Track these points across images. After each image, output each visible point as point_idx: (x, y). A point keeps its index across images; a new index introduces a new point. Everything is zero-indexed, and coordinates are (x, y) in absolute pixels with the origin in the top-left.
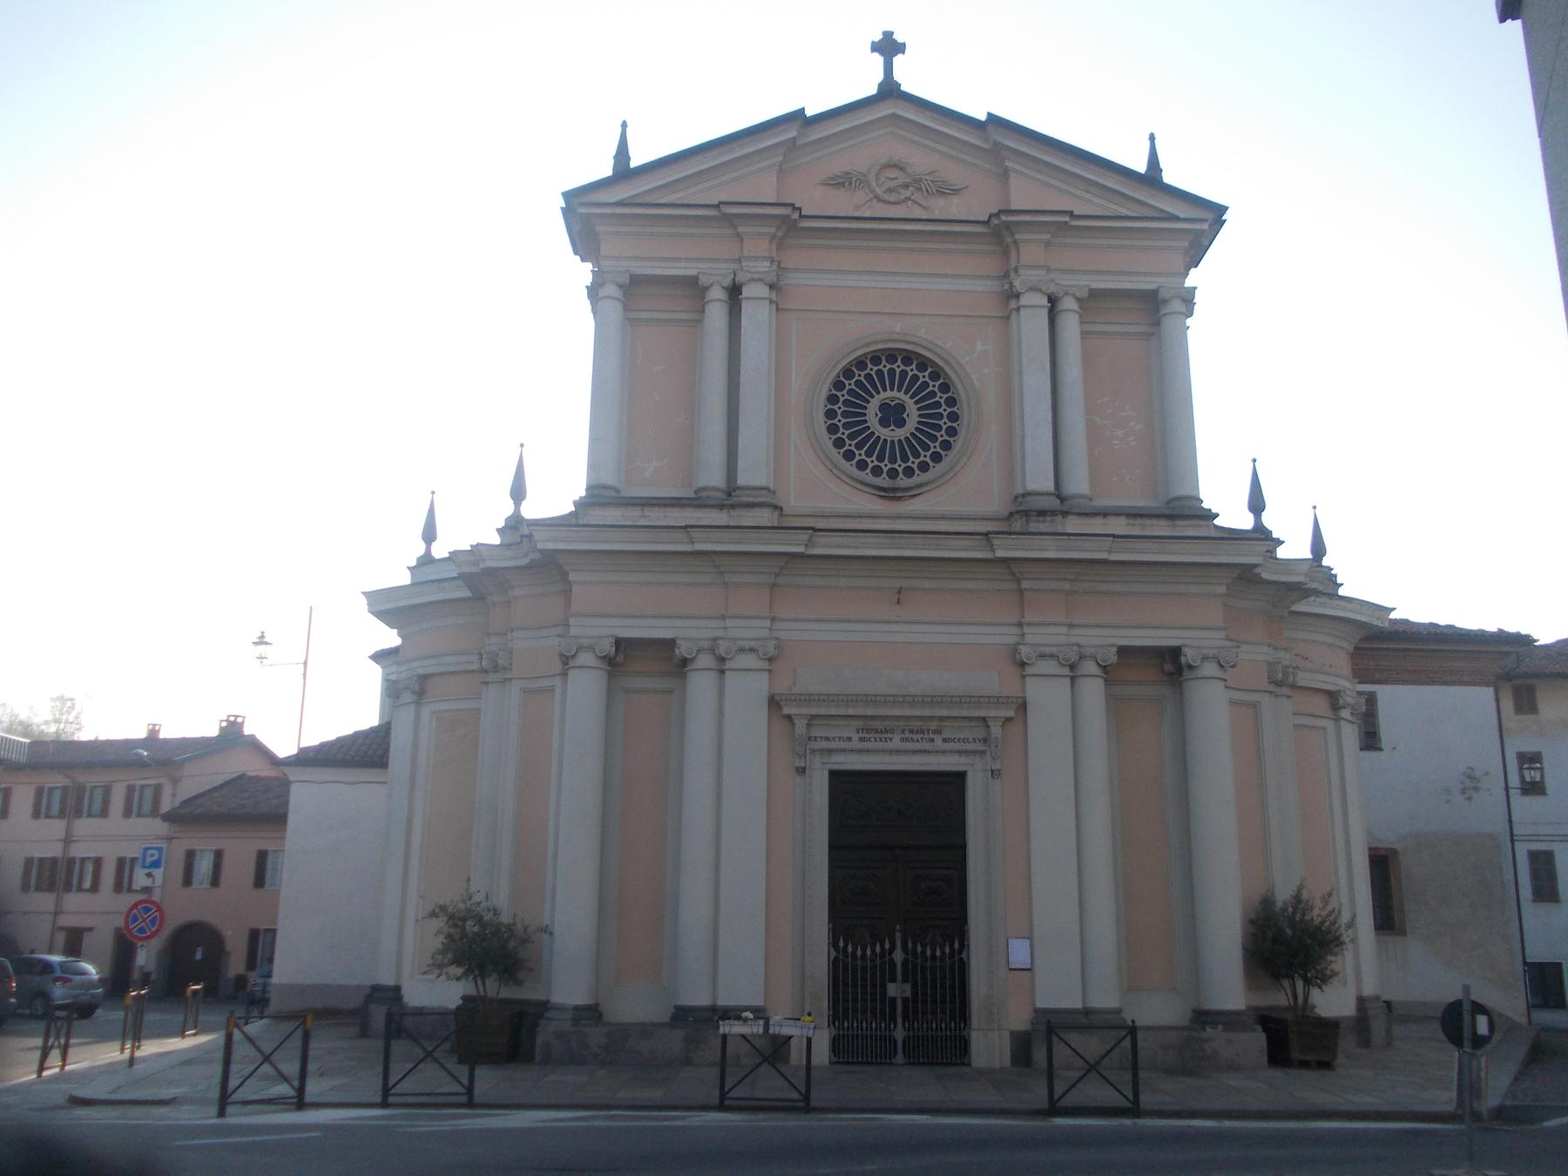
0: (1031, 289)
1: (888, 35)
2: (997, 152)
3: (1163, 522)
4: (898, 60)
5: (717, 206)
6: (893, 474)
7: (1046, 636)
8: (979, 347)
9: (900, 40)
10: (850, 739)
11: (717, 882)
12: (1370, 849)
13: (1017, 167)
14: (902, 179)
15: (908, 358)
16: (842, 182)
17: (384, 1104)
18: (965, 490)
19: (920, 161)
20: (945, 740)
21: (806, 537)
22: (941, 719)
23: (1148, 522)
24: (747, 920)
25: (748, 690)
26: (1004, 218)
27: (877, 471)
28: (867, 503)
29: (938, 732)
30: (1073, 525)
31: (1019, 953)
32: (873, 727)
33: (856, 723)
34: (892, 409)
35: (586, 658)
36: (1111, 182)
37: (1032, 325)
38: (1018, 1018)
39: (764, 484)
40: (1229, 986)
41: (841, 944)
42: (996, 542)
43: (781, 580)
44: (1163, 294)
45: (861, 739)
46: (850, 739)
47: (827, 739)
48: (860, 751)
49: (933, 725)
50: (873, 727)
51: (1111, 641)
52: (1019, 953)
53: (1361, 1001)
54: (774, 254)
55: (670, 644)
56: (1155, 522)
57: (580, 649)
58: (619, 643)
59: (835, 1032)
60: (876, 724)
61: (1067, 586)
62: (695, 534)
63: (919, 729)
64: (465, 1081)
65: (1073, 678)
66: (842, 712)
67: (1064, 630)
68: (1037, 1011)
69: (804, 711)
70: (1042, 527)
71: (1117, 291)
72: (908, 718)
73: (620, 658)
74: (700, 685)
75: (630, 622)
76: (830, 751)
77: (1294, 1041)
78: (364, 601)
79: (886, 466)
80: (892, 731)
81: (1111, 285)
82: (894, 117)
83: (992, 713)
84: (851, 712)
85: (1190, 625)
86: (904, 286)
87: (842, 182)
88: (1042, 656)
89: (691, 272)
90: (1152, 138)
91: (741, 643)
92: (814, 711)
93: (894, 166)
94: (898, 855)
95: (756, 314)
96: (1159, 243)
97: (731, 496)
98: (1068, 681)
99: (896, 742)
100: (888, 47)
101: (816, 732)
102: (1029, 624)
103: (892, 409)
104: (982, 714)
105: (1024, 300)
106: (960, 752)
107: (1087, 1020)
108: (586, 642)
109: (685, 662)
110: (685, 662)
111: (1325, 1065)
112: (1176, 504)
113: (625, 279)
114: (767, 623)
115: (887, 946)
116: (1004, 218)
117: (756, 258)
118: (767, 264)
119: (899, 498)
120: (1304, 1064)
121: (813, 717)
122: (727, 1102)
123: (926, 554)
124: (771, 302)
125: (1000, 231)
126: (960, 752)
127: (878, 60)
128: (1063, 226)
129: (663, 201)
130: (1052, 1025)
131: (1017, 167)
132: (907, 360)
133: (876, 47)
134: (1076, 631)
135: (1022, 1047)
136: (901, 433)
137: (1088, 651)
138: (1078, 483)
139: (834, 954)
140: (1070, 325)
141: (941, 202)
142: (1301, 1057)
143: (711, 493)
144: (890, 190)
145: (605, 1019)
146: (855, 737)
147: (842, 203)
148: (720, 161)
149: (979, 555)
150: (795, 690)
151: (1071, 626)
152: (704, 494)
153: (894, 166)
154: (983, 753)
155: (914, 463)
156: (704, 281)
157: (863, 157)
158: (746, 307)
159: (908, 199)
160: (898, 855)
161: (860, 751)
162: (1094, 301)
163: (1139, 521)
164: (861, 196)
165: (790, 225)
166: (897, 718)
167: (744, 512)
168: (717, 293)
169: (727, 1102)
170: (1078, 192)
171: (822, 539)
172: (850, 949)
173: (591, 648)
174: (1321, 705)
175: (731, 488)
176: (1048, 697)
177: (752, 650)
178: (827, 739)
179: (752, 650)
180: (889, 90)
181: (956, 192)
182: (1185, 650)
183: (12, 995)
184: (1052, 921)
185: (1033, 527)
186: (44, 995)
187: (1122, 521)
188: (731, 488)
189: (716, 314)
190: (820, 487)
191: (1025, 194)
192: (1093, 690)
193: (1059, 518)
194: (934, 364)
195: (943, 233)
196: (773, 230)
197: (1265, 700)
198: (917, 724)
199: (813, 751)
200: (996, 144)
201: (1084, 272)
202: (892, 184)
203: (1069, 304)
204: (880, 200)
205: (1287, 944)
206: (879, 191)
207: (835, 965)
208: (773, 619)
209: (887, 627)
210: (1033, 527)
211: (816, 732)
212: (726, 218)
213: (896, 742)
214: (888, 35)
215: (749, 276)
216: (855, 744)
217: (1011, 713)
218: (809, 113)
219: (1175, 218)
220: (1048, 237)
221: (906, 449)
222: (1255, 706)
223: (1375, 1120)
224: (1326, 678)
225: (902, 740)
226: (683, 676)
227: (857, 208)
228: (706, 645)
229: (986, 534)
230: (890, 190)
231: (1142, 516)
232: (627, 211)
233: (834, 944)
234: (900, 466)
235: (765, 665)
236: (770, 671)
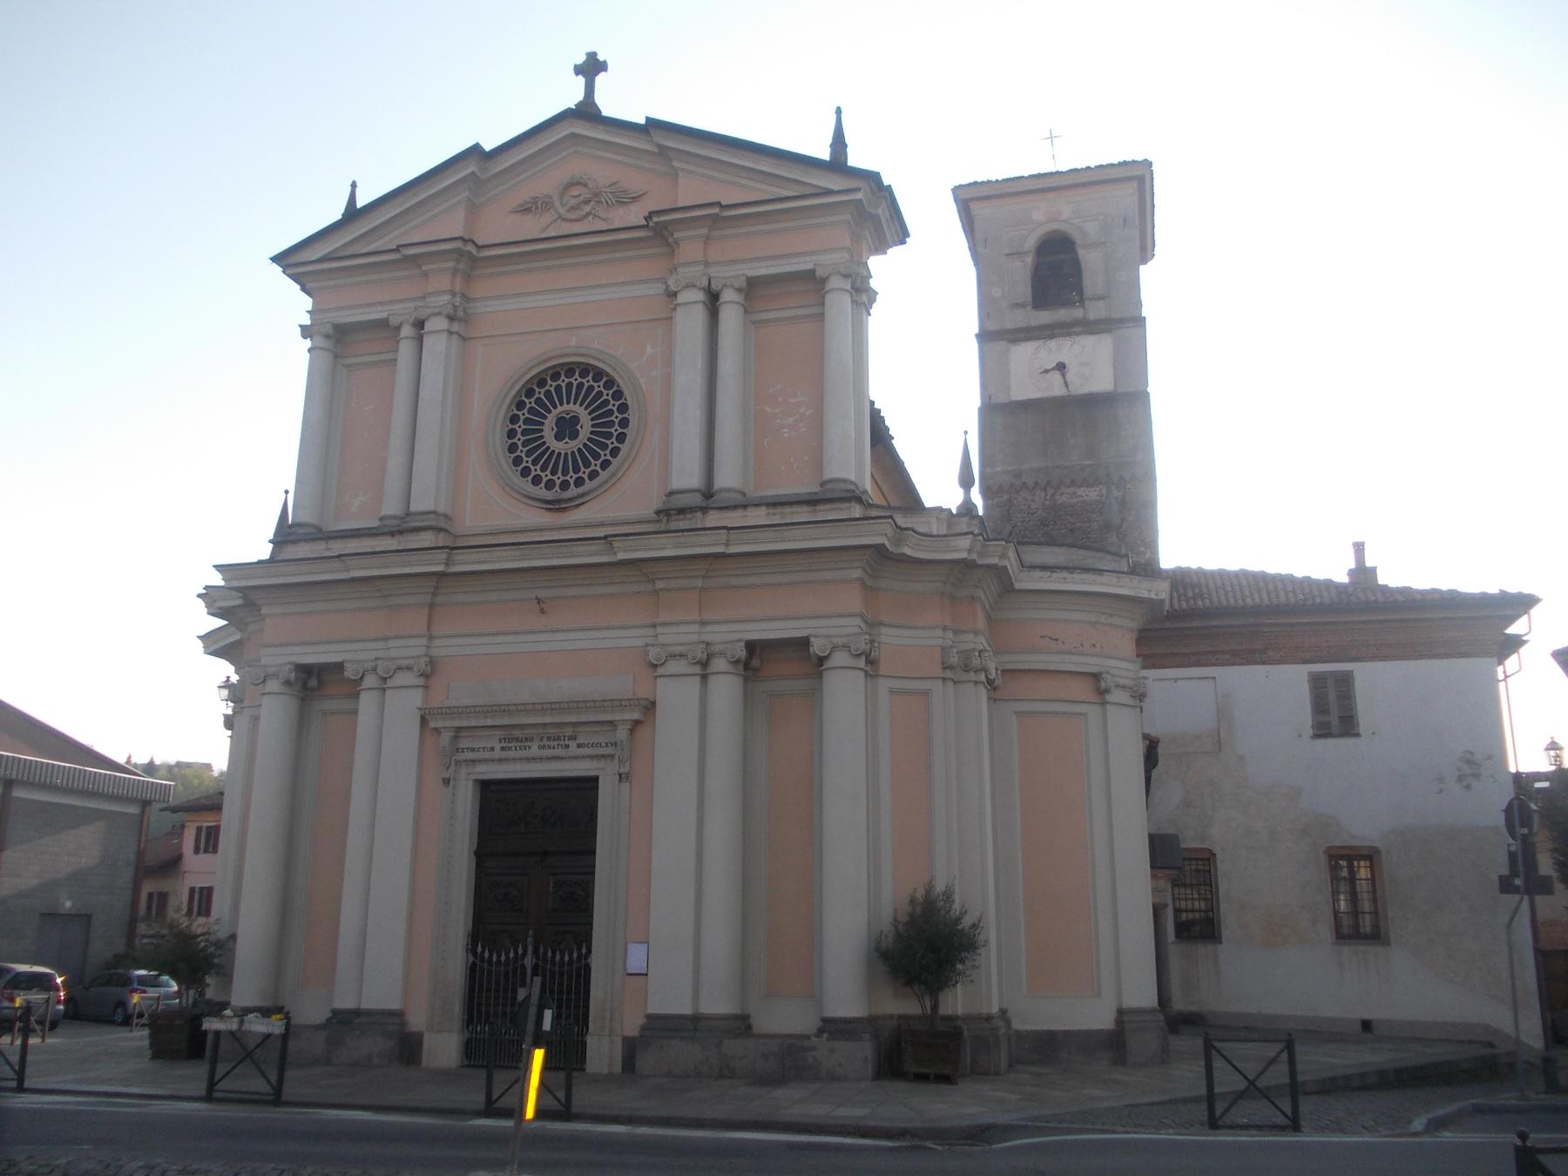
0: (687, 287)
1: (592, 56)
2: (663, 153)
3: (805, 509)
4: (600, 79)
5: (397, 249)
6: (565, 486)
7: (682, 635)
8: (649, 350)
9: (584, 58)
10: (492, 749)
11: (367, 892)
12: (1153, 839)
13: (686, 166)
14: (585, 194)
15: (585, 370)
16: (525, 209)
17: (209, 1098)
18: (624, 497)
19: (602, 173)
20: (579, 746)
21: (444, 556)
22: (575, 724)
23: (787, 509)
24: (390, 923)
25: (405, 704)
26: (655, 219)
27: (550, 485)
28: (536, 517)
29: (573, 738)
30: (713, 519)
31: (636, 958)
32: (513, 736)
33: (499, 733)
34: (567, 420)
35: (719, 664)
36: (765, 166)
37: (690, 321)
38: (631, 1025)
39: (431, 508)
40: (846, 989)
41: (479, 949)
42: (616, 545)
43: (439, 599)
44: (820, 273)
45: (503, 749)
46: (492, 749)
47: (473, 750)
48: (500, 760)
49: (569, 731)
50: (513, 736)
51: (738, 636)
52: (636, 958)
53: (1121, 1012)
54: (458, 288)
55: (804, 642)
56: (795, 509)
57: (834, 648)
58: (751, 646)
59: (467, 1036)
60: (517, 733)
61: (699, 583)
62: (734, 535)
63: (557, 735)
64: (274, 1078)
65: (704, 677)
66: (481, 723)
67: (696, 628)
68: (650, 1017)
69: (449, 723)
70: (683, 525)
71: (772, 276)
72: (545, 725)
73: (755, 662)
74: (367, 702)
75: (308, 649)
76: (473, 761)
77: (922, 1050)
78: (200, 644)
79: (571, 477)
80: (532, 740)
81: (772, 271)
82: (573, 135)
83: (617, 717)
84: (489, 722)
85: (824, 614)
86: (581, 299)
87: (525, 209)
88: (672, 656)
89: (384, 315)
90: (839, 111)
91: (399, 662)
92: (457, 724)
93: (578, 183)
94: (535, 857)
95: (437, 346)
96: (815, 221)
97: (401, 526)
98: (697, 679)
99: (534, 750)
100: (591, 68)
101: (464, 744)
102: (664, 624)
103: (567, 420)
104: (609, 717)
105: (681, 298)
106: (591, 757)
107: (690, 1026)
108: (840, 641)
109: (821, 660)
110: (821, 660)
111: (946, 1079)
112: (829, 486)
113: (328, 329)
114: (424, 641)
115: (520, 951)
116: (655, 219)
117: (438, 293)
118: (447, 297)
119: (564, 510)
120: (921, 1078)
121: (459, 729)
122: (216, 1095)
123: (555, 562)
124: (450, 333)
125: (660, 232)
126: (591, 757)
127: (581, 81)
128: (718, 218)
129: (365, 251)
130: (661, 1027)
131: (686, 166)
132: (570, 372)
133: (579, 70)
134: (709, 628)
135: (631, 1049)
136: (574, 445)
137: (717, 648)
138: (728, 477)
139: (471, 959)
140: (731, 317)
141: (621, 211)
142: (915, 1069)
143: (727, 495)
144: (573, 208)
145: (756, 1030)
146: (498, 746)
147: (531, 227)
148: (407, 205)
149: (605, 559)
150: (448, 703)
151: (702, 623)
152: (829, 486)
153: (578, 183)
154: (612, 756)
155: (584, 473)
156: (393, 322)
157: (546, 182)
158: (427, 341)
159: (589, 214)
160: (535, 857)
161: (500, 760)
162: (753, 289)
163: (779, 510)
164: (547, 218)
165: (470, 258)
166: (534, 726)
167: (411, 537)
168: (407, 331)
169: (216, 1095)
170: (743, 181)
171: (459, 556)
172: (487, 955)
173: (275, 675)
174: (1081, 689)
175: (708, 493)
176: (677, 697)
177: (682, 655)
178: (473, 750)
179: (682, 655)
180: (586, 111)
181: (635, 199)
182: (812, 639)
183: (59, 1002)
184: (670, 927)
185: (674, 525)
186: (122, 1004)
187: (763, 511)
188: (708, 493)
189: (406, 350)
190: (494, 504)
191: (692, 190)
192: (726, 688)
193: (699, 514)
194: (608, 375)
195: (612, 244)
196: (451, 264)
197: (936, 687)
198: (552, 731)
199: (458, 763)
200: (660, 146)
201: (744, 261)
202: (573, 202)
203: (728, 295)
204: (564, 220)
205: (926, 947)
206: (562, 211)
207: (472, 970)
208: (431, 638)
209: (532, 637)
210: (674, 525)
211: (464, 744)
212: (409, 260)
213: (534, 750)
214: (592, 56)
215: (429, 311)
216: (498, 754)
217: (636, 716)
218: (488, 147)
219: (829, 192)
220: (705, 231)
221: (581, 460)
222: (925, 694)
223: (863, 1136)
224: (1083, 659)
225: (540, 747)
226: (820, 676)
227: (544, 230)
228: (369, 665)
229: (606, 537)
230: (573, 208)
231: (783, 504)
232: (326, 266)
233: (472, 948)
234: (571, 477)
235: (421, 681)
236: (426, 687)
